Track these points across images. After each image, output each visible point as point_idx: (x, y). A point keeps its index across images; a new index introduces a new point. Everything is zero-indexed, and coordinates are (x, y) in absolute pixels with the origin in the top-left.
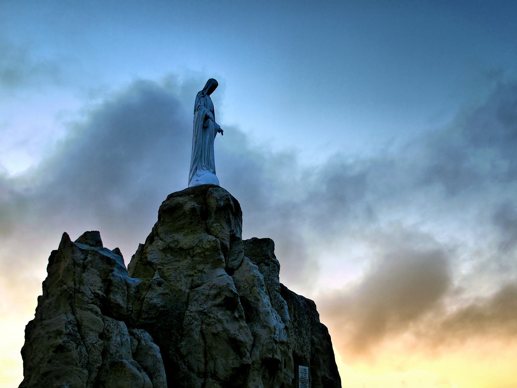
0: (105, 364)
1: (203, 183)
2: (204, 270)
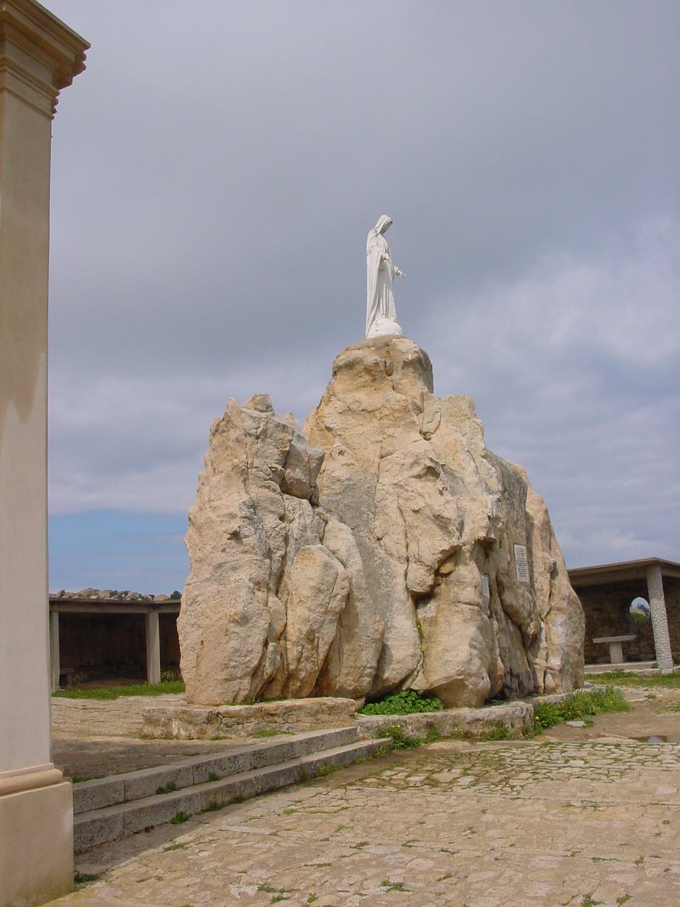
0: (290, 552)
1: (384, 333)
2: (395, 435)
